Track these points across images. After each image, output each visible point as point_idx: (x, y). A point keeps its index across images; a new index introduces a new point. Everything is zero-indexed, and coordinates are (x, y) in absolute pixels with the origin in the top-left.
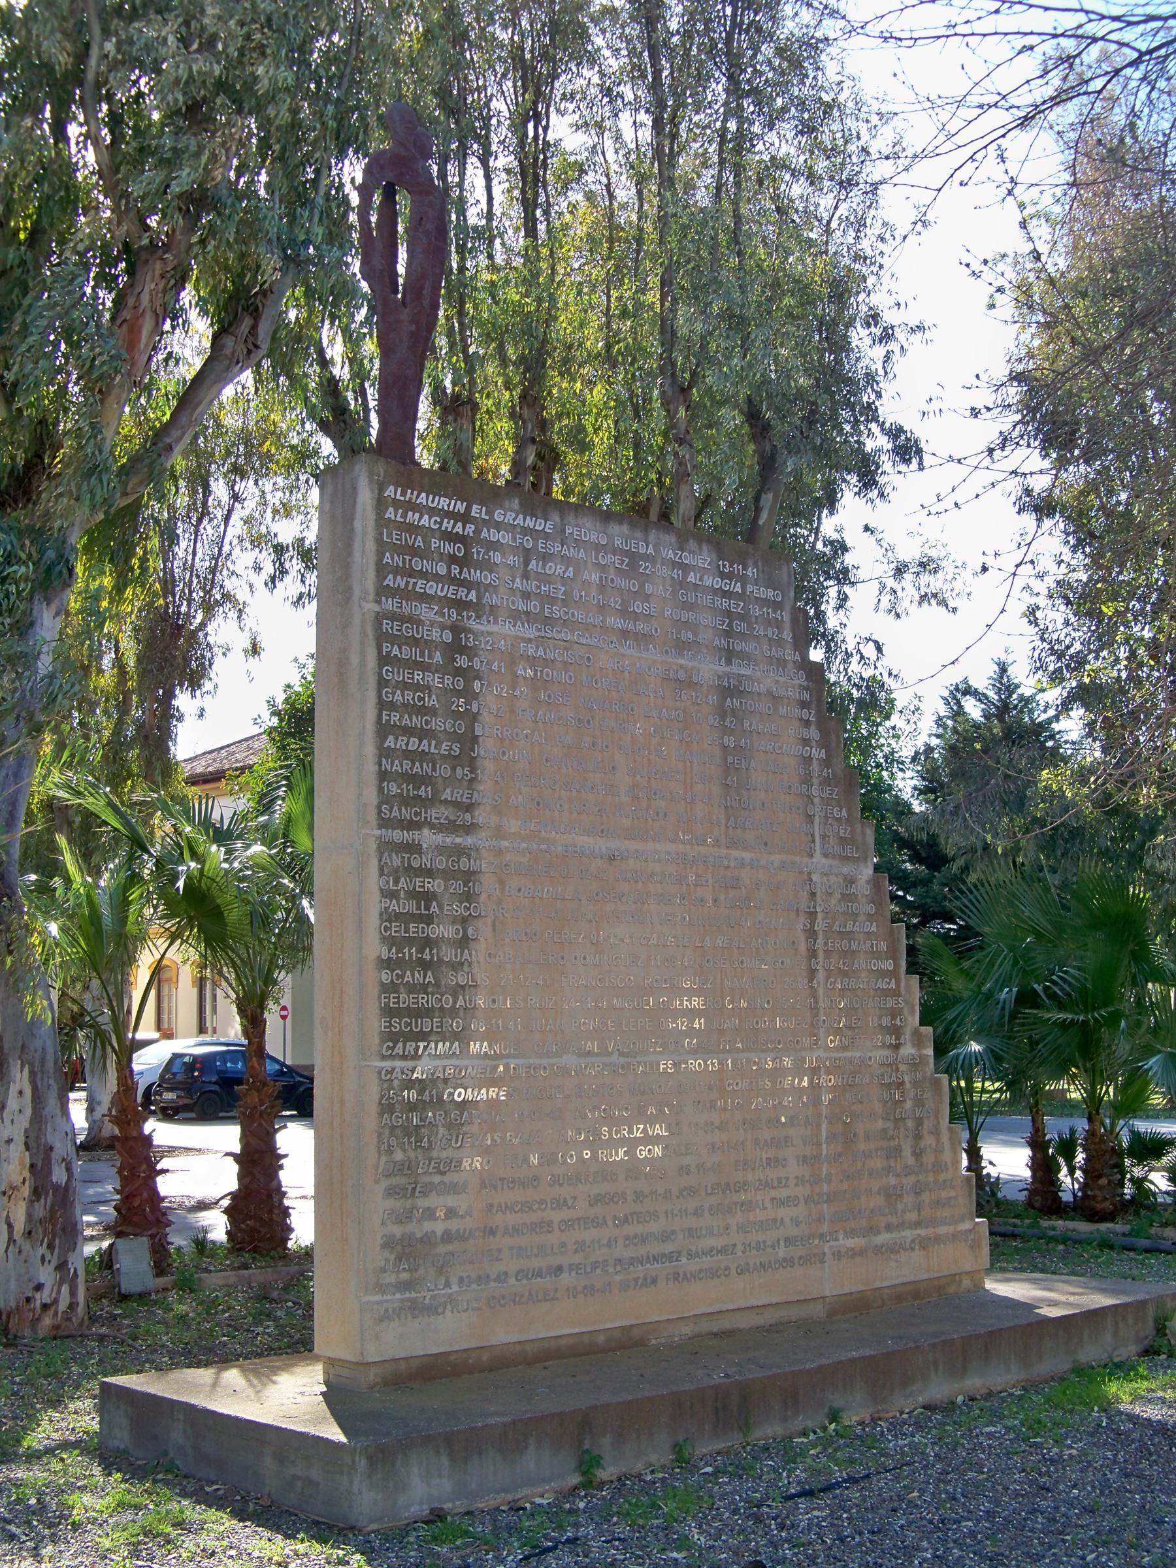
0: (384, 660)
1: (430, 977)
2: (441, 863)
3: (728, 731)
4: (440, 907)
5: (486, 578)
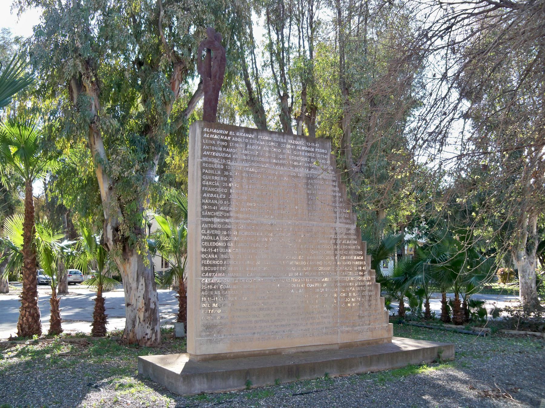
0: (203, 174)
1: (216, 256)
2: (219, 226)
3: (308, 189)
4: (219, 238)
5: (234, 151)
